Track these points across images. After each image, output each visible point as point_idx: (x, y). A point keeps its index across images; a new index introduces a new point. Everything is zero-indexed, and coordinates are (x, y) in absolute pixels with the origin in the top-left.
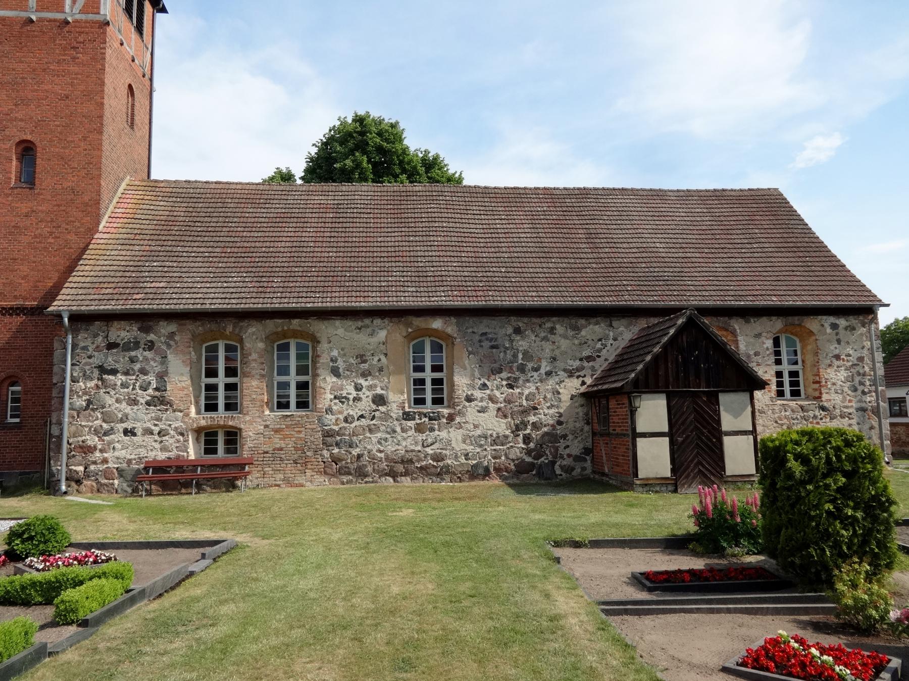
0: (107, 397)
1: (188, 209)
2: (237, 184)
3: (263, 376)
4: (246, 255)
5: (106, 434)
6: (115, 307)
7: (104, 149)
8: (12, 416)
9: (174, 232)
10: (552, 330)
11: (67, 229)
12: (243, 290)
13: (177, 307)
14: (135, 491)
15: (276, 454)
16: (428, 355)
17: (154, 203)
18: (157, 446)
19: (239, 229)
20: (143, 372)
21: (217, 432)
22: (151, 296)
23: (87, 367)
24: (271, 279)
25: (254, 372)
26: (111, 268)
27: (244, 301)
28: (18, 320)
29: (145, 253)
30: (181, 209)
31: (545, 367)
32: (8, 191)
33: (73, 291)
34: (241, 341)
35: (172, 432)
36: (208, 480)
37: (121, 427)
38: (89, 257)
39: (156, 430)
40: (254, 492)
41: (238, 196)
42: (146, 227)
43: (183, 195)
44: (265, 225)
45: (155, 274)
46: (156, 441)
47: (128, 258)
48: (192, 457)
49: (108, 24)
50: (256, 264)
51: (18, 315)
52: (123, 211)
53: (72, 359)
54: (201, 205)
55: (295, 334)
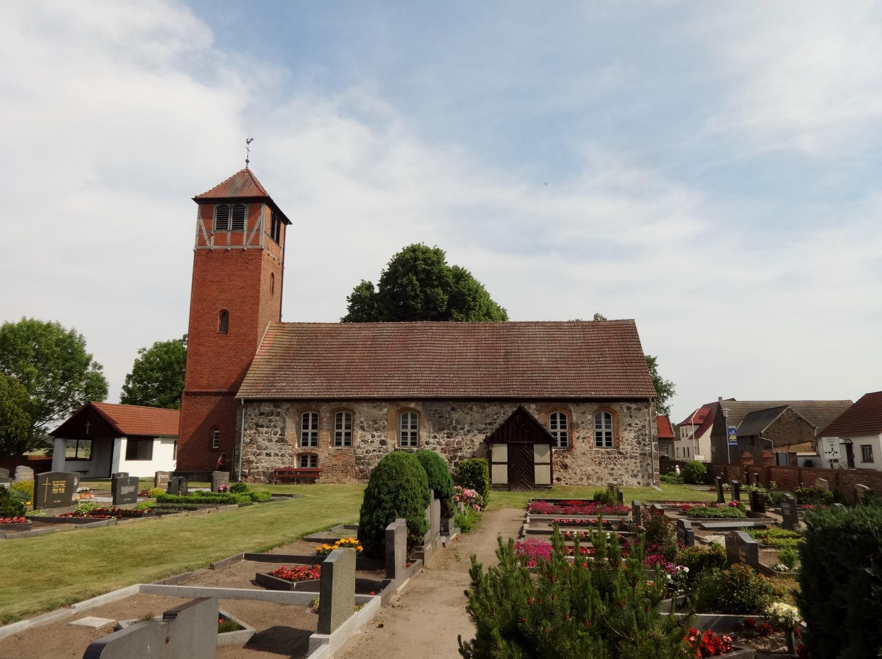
3: (328, 430)
5: (258, 455)
10: (471, 409)
15: (333, 468)
16: (409, 420)
20: (275, 426)
28: (219, 398)
31: (467, 428)
36: (302, 478)
37: (264, 452)
48: (296, 467)
55: (345, 409)
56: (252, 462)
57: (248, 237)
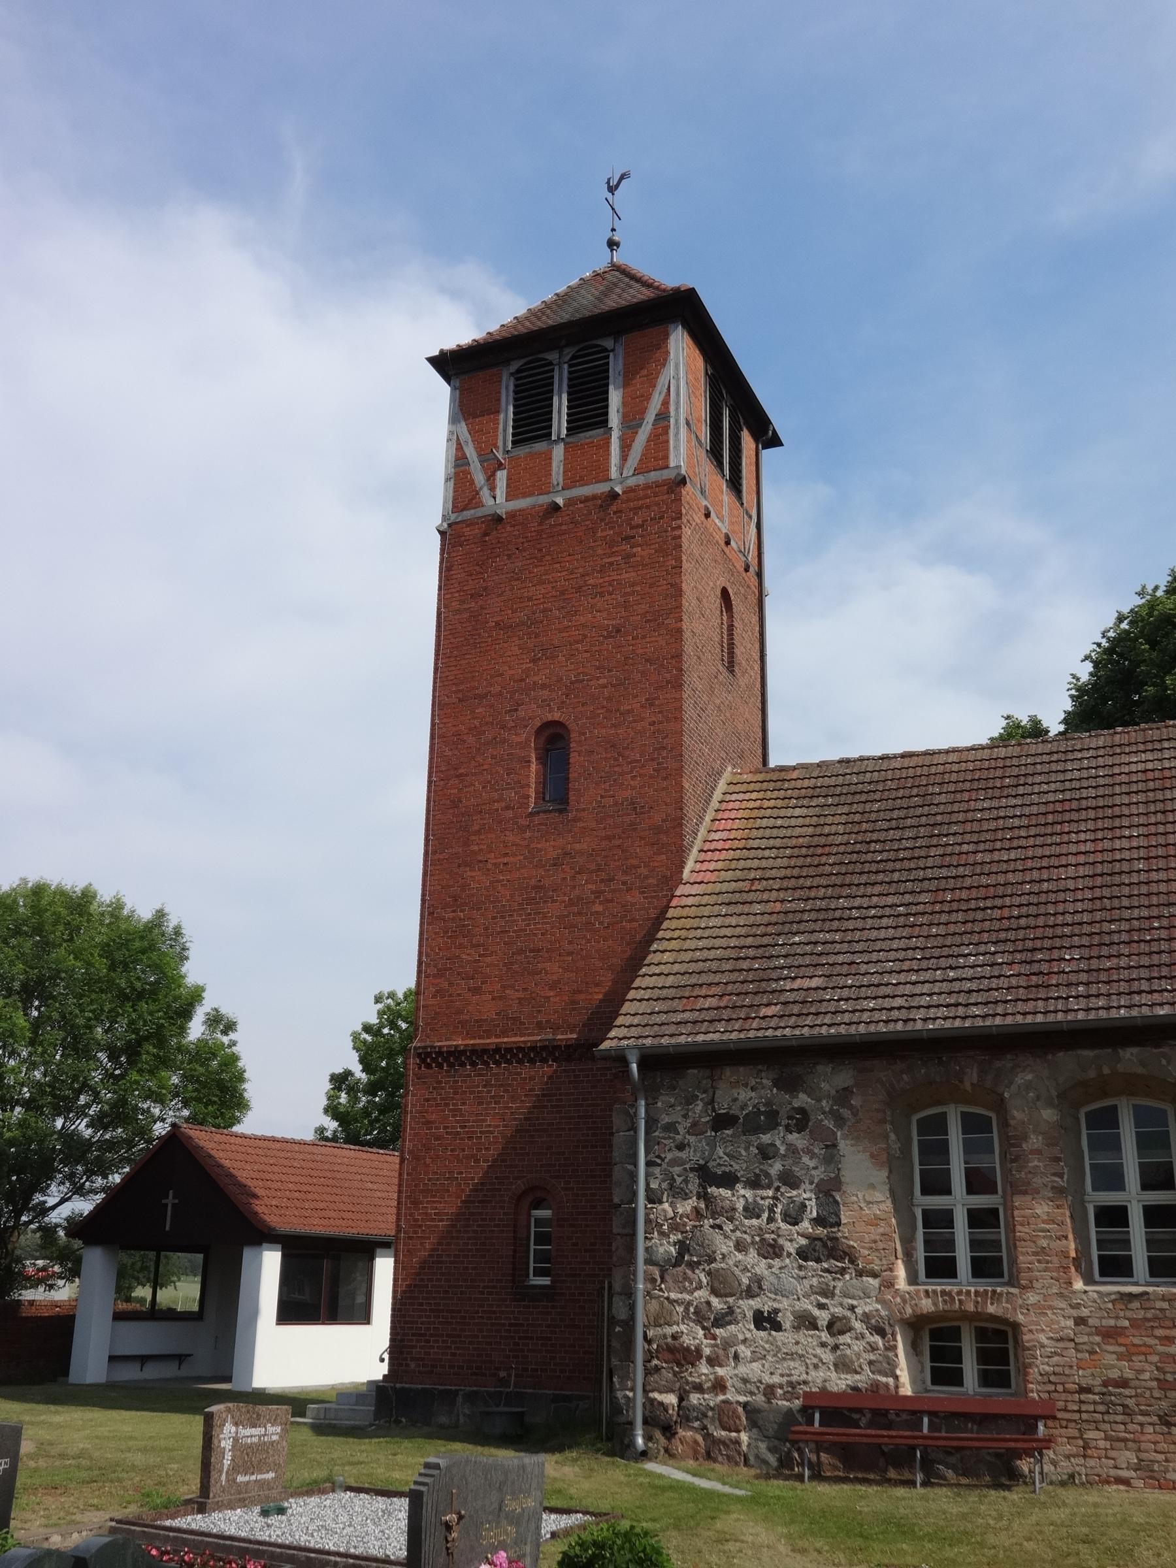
0: (718, 1237)
1: (851, 818)
2: (947, 752)
3: (1059, 1191)
4: (989, 903)
5: (720, 1322)
6: (725, 1037)
7: (686, 716)
8: (539, 1272)
9: (828, 869)
11: (624, 883)
12: (994, 983)
13: (853, 1030)
14: (785, 1462)
17: (783, 813)
18: (827, 1356)
19: (965, 848)
20: (790, 1180)
21: (958, 1330)
22: (796, 1009)
23: (677, 1170)
24: (1056, 954)
25: (1037, 1181)
26: (712, 954)
27: (1000, 1009)
28: (547, 1070)
29: (774, 918)
30: (837, 819)
32: (524, 822)
33: (643, 1007)
34: (1000, 1106)
35: (858, 1325)
36: (948, 1452)
37: (748, 1306)
38: (668, 935)
39: (823, 1317)
40: (1069, 1495)
41: (954, 777)
42: (770, 863)
43: (838, 790)
44: (1023, 833)
45: (800, 961)
46: (823, 1345)
47: (743, 931)
48: (907, 1390)
49: (683, 481)
50: (1014, 923)
51: (544, 1061)
52: (724, 835)
53: (647, 1153)
54: (876, 806)
55: (1132, 1085)
56: (690, 1357)
57: (626, 447)
